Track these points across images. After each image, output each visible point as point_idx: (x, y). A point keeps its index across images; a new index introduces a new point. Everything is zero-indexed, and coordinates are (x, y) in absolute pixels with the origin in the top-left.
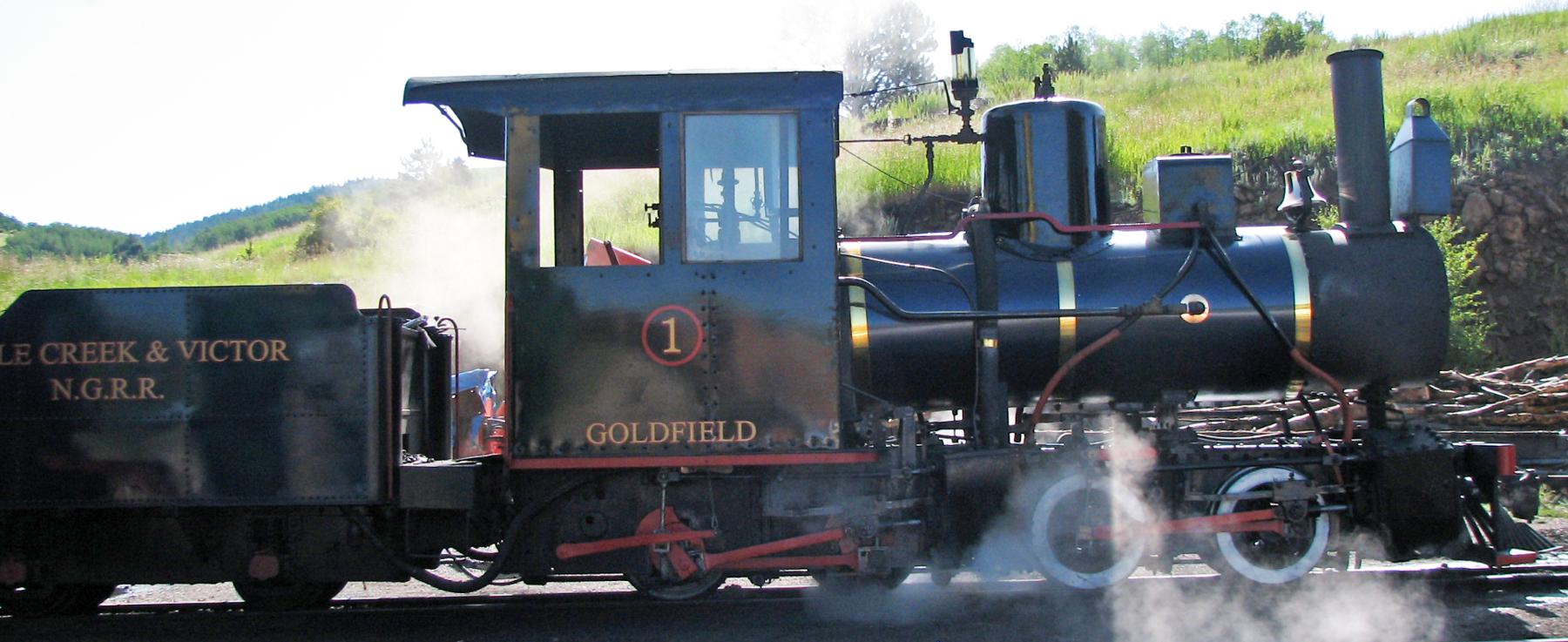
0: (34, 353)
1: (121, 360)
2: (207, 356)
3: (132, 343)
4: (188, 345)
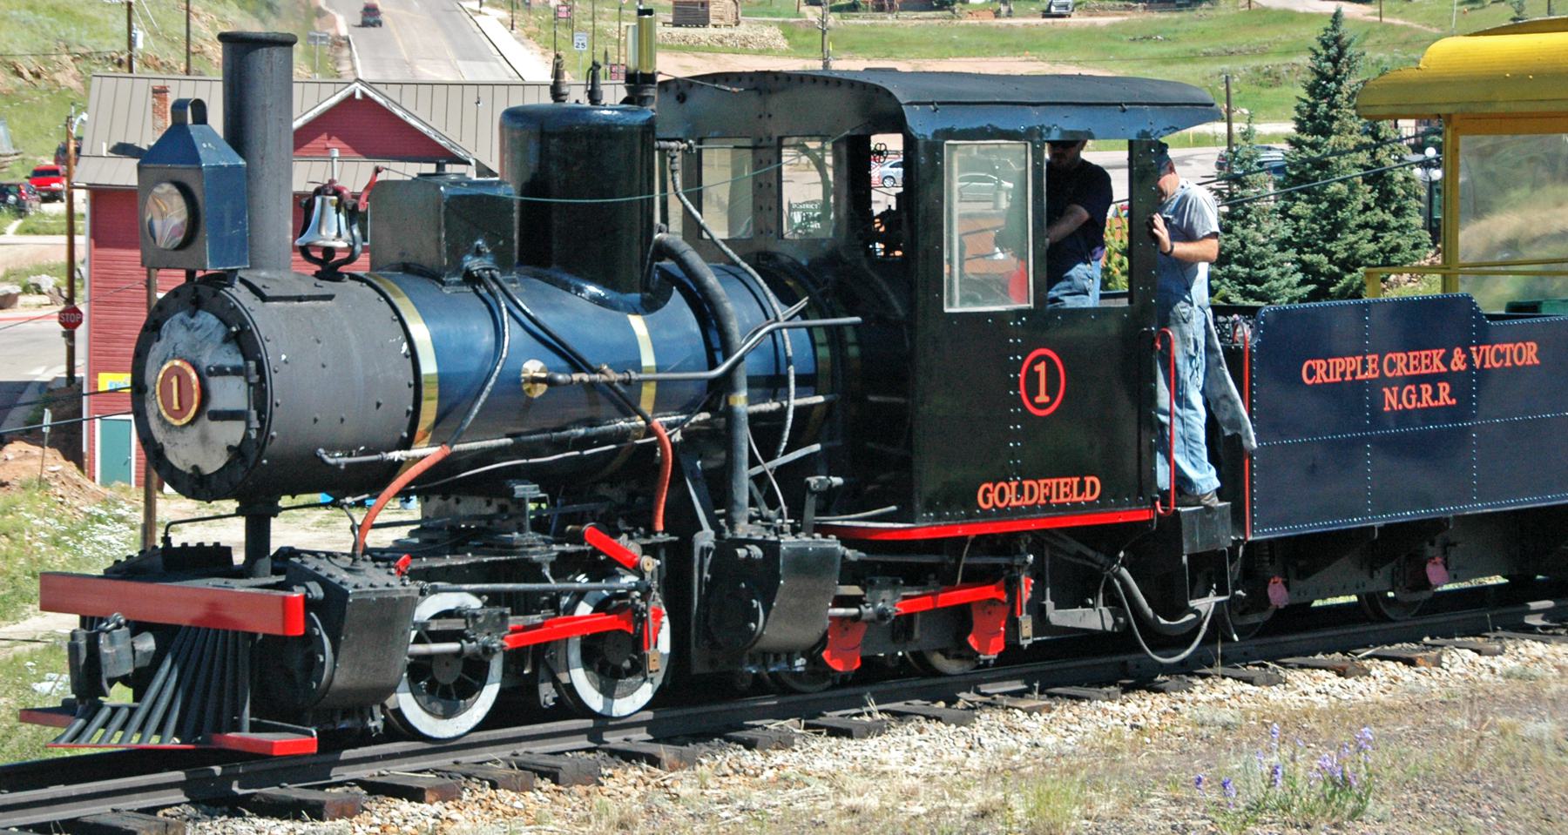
2: (1512, 360)
4: (1478, 352)
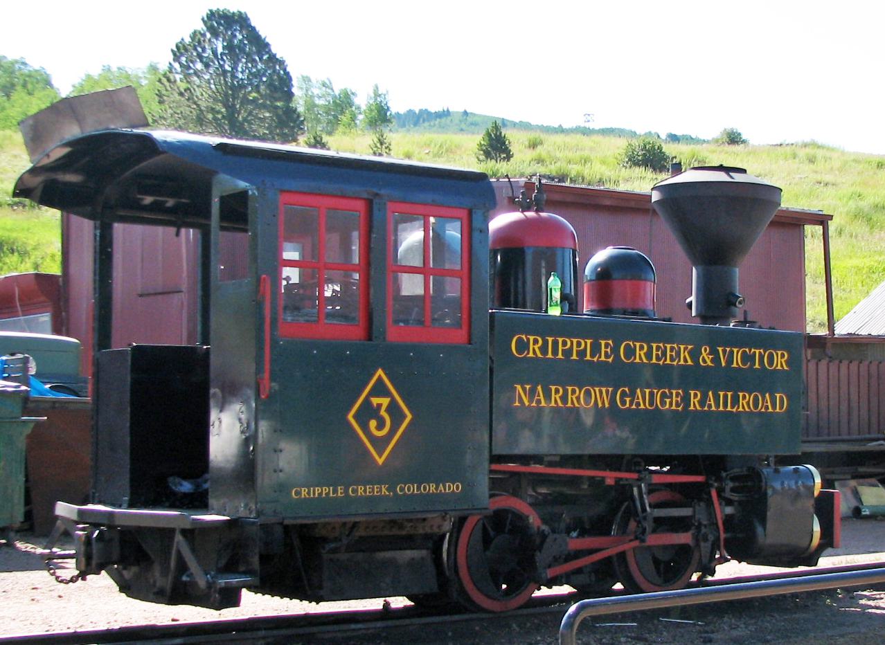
0: (615, 350)
1: (682, 362)
3: (690, 347)
4: (724, 352)
